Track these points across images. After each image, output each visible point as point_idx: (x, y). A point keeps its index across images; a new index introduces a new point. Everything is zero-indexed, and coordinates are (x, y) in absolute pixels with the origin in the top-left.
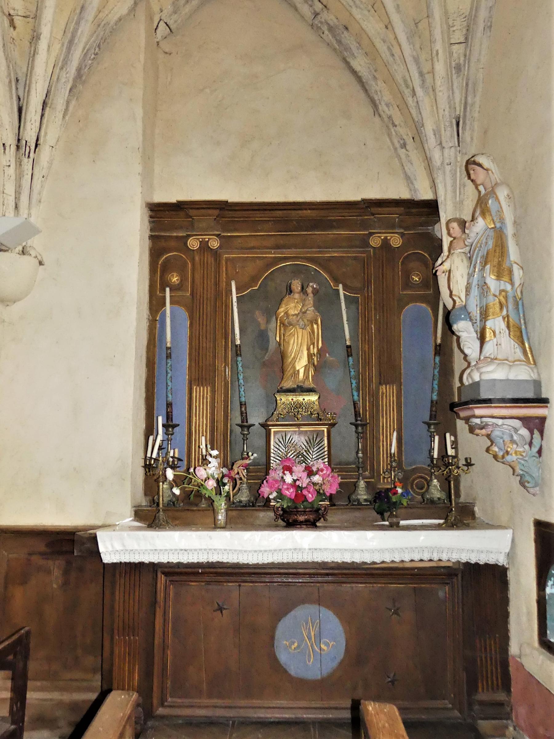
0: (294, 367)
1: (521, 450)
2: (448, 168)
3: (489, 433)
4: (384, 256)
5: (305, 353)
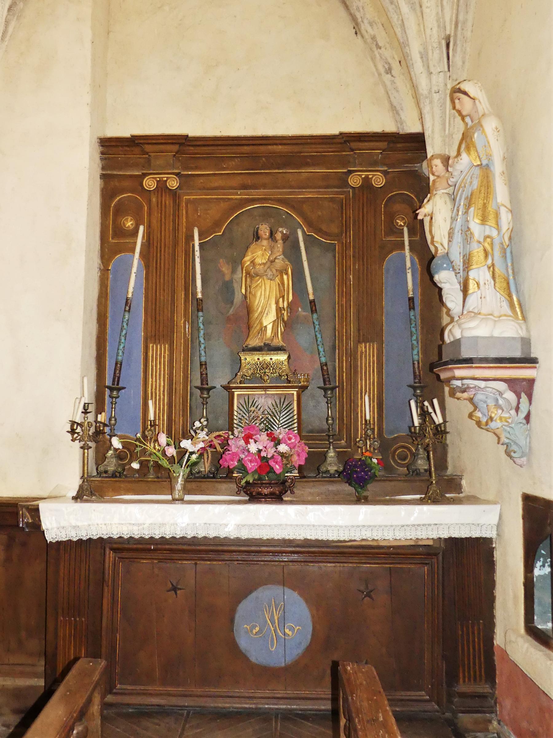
0: (261, 323)
1: (507, 415)
2: (436, 97)
3: (472, 396)
4: (365, 197)
5: (274, 306)
